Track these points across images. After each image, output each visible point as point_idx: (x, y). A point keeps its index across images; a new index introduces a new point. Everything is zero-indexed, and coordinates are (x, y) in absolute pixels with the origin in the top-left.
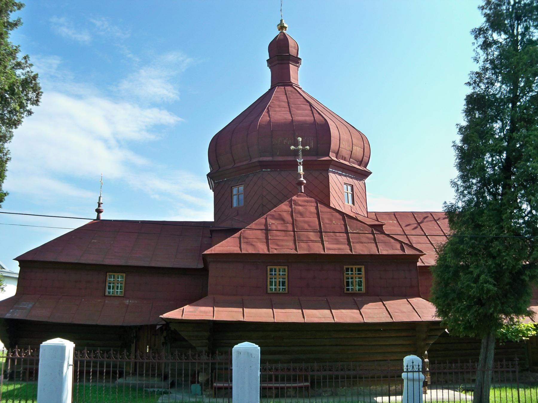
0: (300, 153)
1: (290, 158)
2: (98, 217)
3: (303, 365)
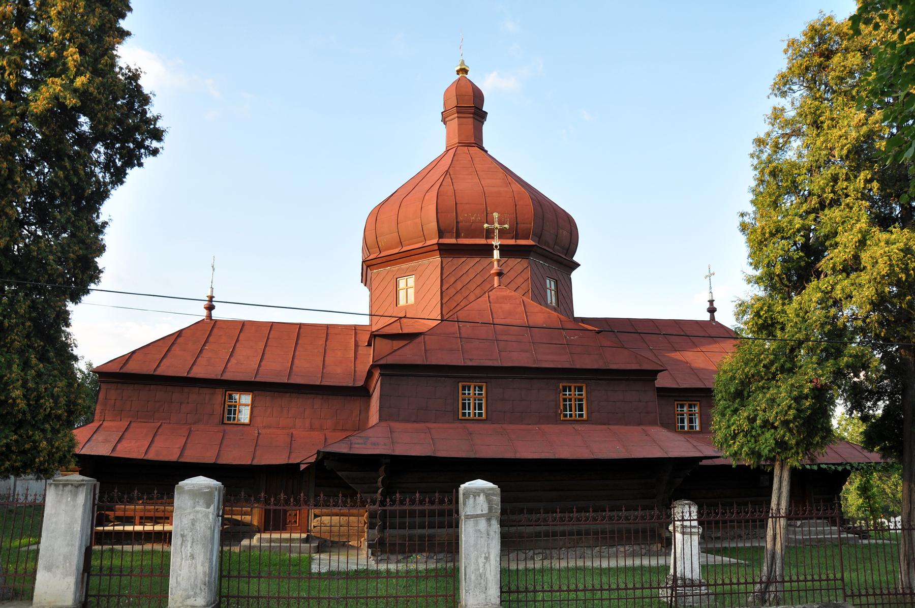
1: (483, 241)
2: (209, 316)
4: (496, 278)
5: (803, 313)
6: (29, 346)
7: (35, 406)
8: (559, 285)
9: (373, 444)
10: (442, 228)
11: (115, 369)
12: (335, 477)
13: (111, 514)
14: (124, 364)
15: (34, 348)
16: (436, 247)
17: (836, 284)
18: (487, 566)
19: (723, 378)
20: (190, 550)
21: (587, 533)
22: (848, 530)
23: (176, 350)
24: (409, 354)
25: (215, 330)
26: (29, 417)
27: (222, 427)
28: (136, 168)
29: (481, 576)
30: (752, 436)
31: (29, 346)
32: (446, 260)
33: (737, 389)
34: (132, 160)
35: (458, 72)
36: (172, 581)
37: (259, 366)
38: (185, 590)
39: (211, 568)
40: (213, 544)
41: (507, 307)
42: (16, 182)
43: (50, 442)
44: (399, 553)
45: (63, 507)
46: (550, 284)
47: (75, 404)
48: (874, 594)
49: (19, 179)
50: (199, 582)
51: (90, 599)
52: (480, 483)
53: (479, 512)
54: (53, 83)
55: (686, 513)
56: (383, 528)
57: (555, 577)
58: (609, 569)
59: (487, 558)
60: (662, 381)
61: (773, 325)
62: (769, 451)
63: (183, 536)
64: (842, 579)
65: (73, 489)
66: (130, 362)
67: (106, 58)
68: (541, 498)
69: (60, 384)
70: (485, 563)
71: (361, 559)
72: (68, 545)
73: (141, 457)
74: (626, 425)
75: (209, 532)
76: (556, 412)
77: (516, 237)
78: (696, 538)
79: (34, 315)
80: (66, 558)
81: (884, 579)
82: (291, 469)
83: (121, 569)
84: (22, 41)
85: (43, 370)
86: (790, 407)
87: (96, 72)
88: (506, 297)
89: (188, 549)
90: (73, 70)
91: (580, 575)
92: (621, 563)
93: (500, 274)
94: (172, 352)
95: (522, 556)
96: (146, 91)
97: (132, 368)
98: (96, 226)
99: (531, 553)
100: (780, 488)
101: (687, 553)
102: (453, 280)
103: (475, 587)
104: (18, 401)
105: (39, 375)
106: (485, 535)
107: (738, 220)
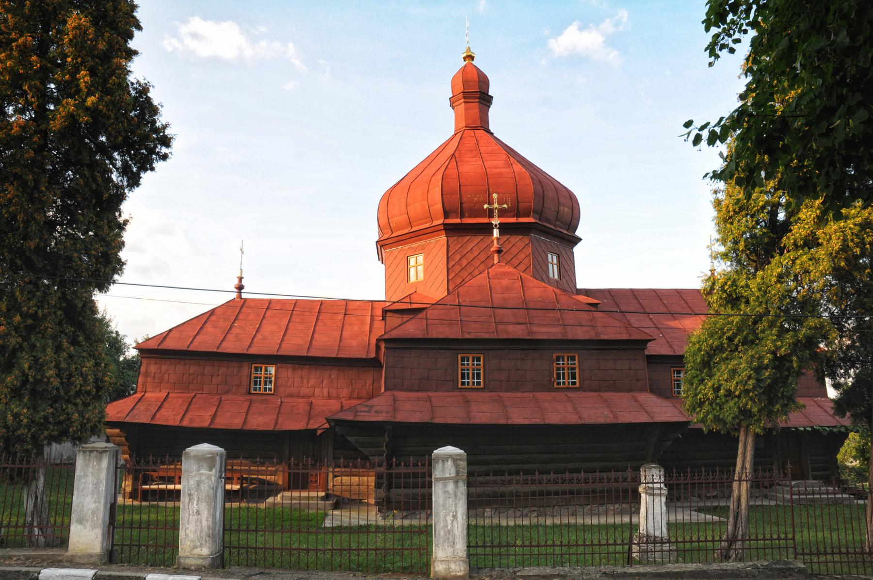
0: (496, 212)
1: (485, 220)
3: (613, 474)
4: (496, 255)
5: (764, 289)
6: (61, 332)
7: (67, 383)
8: (562, 259)
9: (377, 412)
10: (447, 209)
11: (153, 345)
12: (344, 441)
13: (155, 474)
14: (162, 342)
15: (66, 334)
16: (442, 227)
17: (796, 259)
18: (455, 523)
19: (692, 350)
20: (196, 507)
21: (579, 493)
22: (844, 491)
23: (209, 328)
24: (412, 328)
25: (244, 309)
26: (62, 393)
27: (248, 397)
28: (149, 172)
29: (449, 532)
30: (717, 404)
31: (61, 332)
32: (451, 239)
33: (703, 360)
34: (146, 164)
35: (465, 59)
36: (182, 534)
37: (282, 340)
38: (192, 541)
39: (214, 523)
40: (215, 502)
41: (505, 282)
42: (41, 192)
43: (81, 414)
44: (404, 510)
45: (90, 470)
46: (552, 259)
47: (102, 381)
48: (840, 553)
49: (43, 189)
50: (204, 535)
51: (116, 548)
52: (450, 450)
53: (447, 475)
54: (67, 103)
55: (653, 476)
56: (390, 487)
57: (496, 534)
58: (599, 526)
59: (455, 517)
60: (653, 349)
61: (738, 299)
62: (733, 418)
63: (190, 495)
64: (793, 539)
65: (98, 454)
66: (168, 339)
67: (114, 78)
68: (506, 463)
69: (88, 365)
70: (453, 521)
71: (372, 517)
72: (95, 502)
73: (177, 424)
74: (617, 391)
75: (211, 492)
76: (550, 380)
77: (518, 215)
78: (664, 499)
79: (64, 305)
80: (93, 513)
81: (857, 538)
82: (308, 435)
83: (132, 523)
84: (41, 67)
85: (73, 352)
86: (750, 377)
87: (106, 91)
88: (506, 274)
89: (194, 506)
90: (85, 90)
91: (519, 532)
92: (611, 520)
93: (499, 251)
94: (205, 329)
95: (518, 513)
96: (155, 102)
97: (169, 345)
98: (120, 224)
99: (526, 511)
100: (744, 453)
101: (653, 513)
102: (458, 257)
103: (444, 541)
104: (52, 380)
105: (71, 356)
106: (453, 496)
107: (712, 197)
